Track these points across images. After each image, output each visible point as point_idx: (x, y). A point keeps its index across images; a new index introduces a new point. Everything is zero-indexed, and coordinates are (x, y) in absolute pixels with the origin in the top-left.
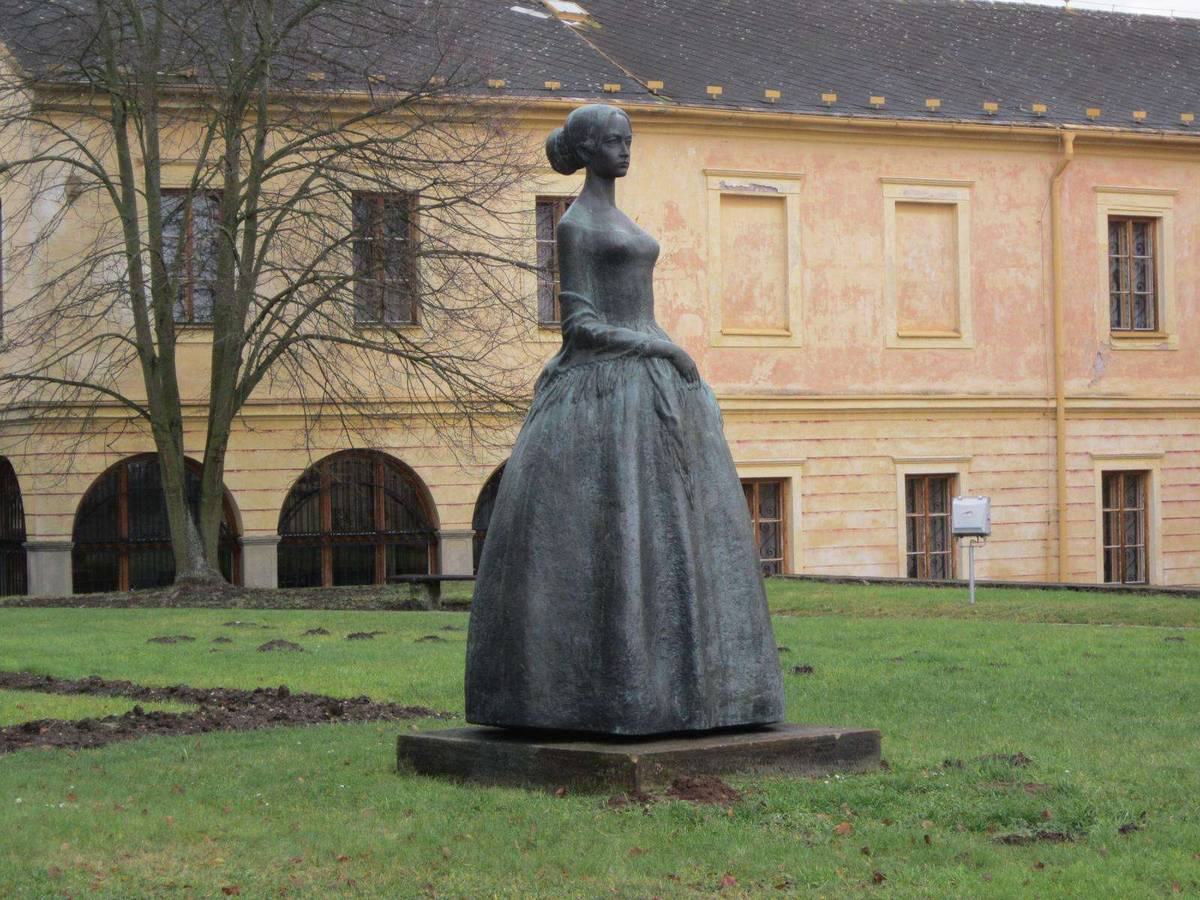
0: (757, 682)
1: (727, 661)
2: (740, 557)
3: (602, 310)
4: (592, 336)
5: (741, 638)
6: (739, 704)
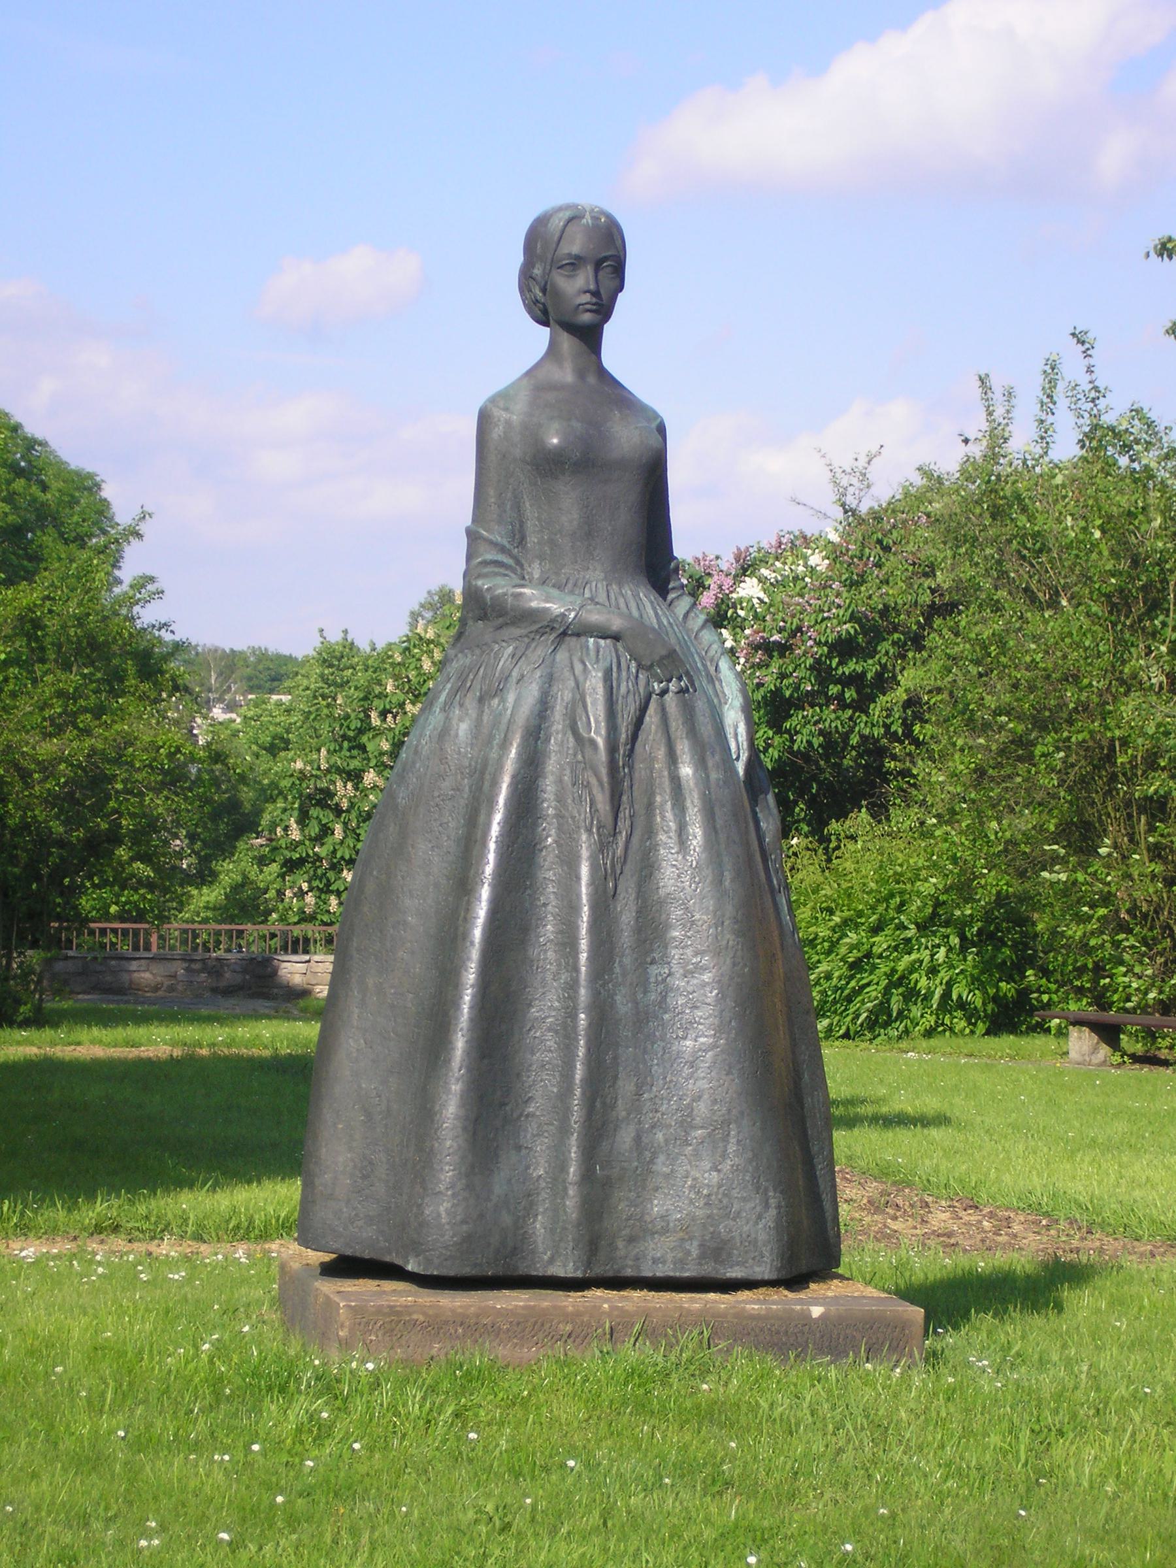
4: (483, 597)
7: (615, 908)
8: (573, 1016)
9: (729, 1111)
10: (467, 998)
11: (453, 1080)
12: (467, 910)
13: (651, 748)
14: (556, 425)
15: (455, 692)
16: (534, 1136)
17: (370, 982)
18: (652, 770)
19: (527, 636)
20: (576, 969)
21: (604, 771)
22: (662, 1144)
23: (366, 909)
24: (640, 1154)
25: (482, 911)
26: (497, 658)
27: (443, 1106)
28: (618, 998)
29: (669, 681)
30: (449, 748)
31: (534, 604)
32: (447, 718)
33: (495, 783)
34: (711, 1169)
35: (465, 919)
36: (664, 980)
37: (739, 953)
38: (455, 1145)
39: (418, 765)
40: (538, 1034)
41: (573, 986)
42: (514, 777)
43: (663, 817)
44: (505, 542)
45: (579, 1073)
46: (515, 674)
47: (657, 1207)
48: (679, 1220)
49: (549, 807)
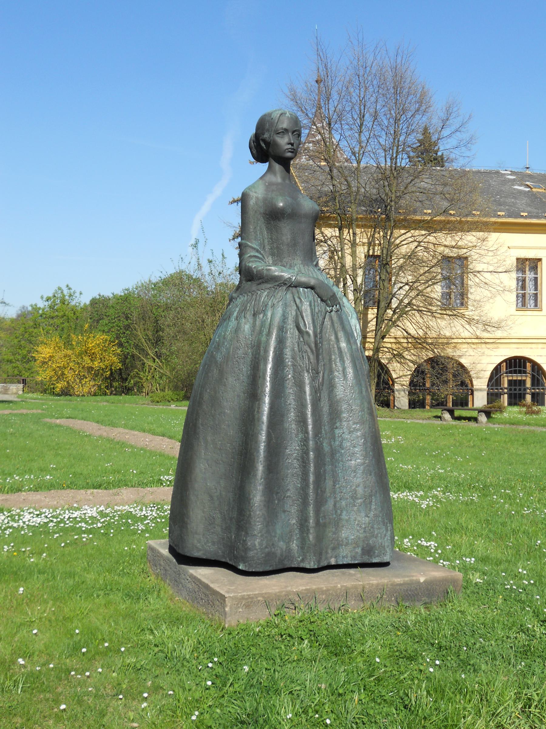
0: (365, 532)
1: (341, 515)
3: (270, 255)
4: (253, 271)
6: (350, 547)
7: (320, 405)
8: (306, 453)
9: (372, 491)
10: (262, 447)
11: (258, 484)
12: (259, 408)
13: (329, 335)
14: (280, 198)
15: (240, 313)
16: (291, 506)
17: (209, 438)
18: (329, 344)
20: (307, 432)
21: (313, 345)
23: (205, 407)
24: (336, 512)
25: (266, 408)
26: (260, 296)
27: (254, 496)
28: (324, 444)
29: (333, 306)
30: (241, 336)
31: (276, 274)
32: (238, 323)
33: (266, 351)
34: (365, 516)
35: (258, 412)
36: (341, 436)
37: (371, 423)
38: (261, 513)
39: (226, 344)
40: (290, 461)
41: (305, 440)
42: (275, 348)
43: (336, 365)
44: (258, 248)
45: (312, 478)
46: (270, 303)
47: (344, 534)
48: (353, 539)
49: (289, 362)
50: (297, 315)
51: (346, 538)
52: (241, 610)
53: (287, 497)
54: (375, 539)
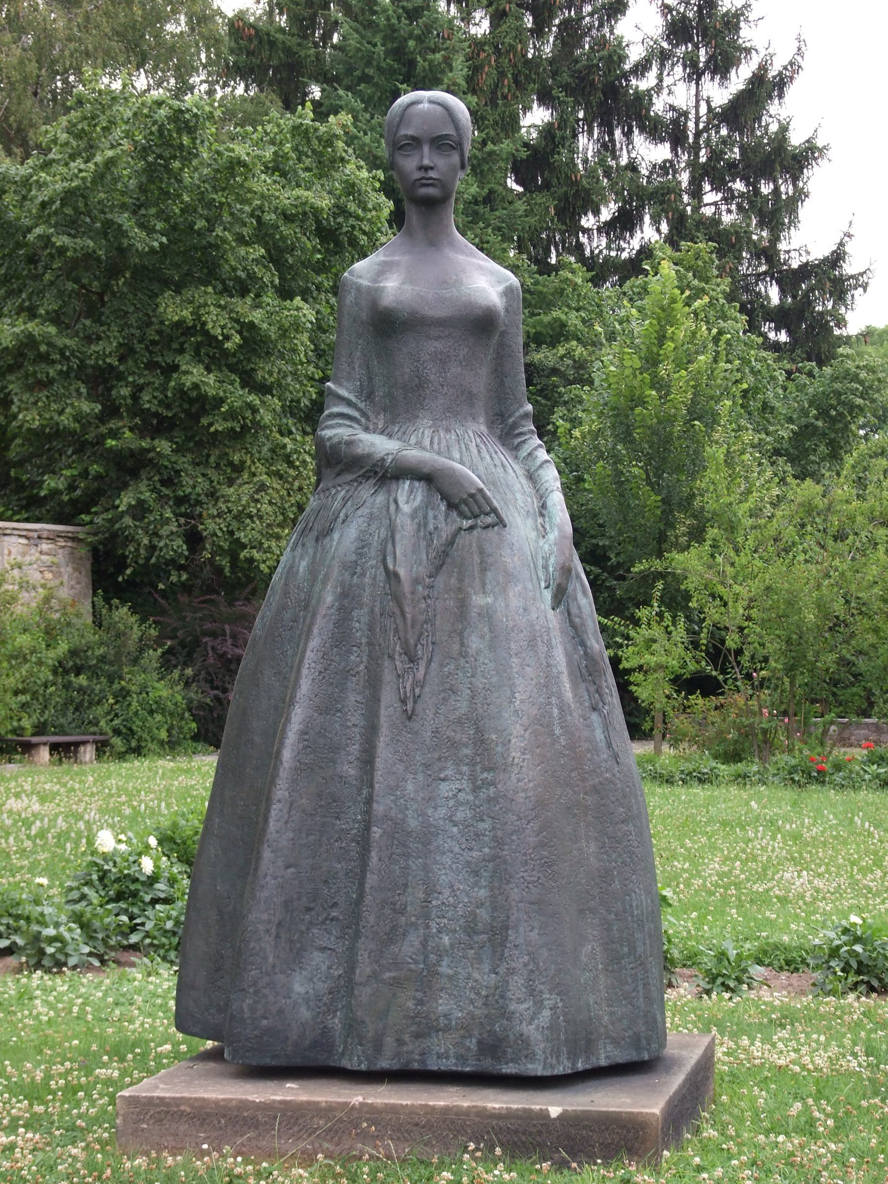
0: (485, 1004)
2: (489, 800)
5: (471, 929)
19: (356, 480)
22: (448, 948)
24: (426, 957)
50: (385, 540)
51: (445, 1016)
52: (145, 1126)
53: (332, 920)
54: (505, 1022)
